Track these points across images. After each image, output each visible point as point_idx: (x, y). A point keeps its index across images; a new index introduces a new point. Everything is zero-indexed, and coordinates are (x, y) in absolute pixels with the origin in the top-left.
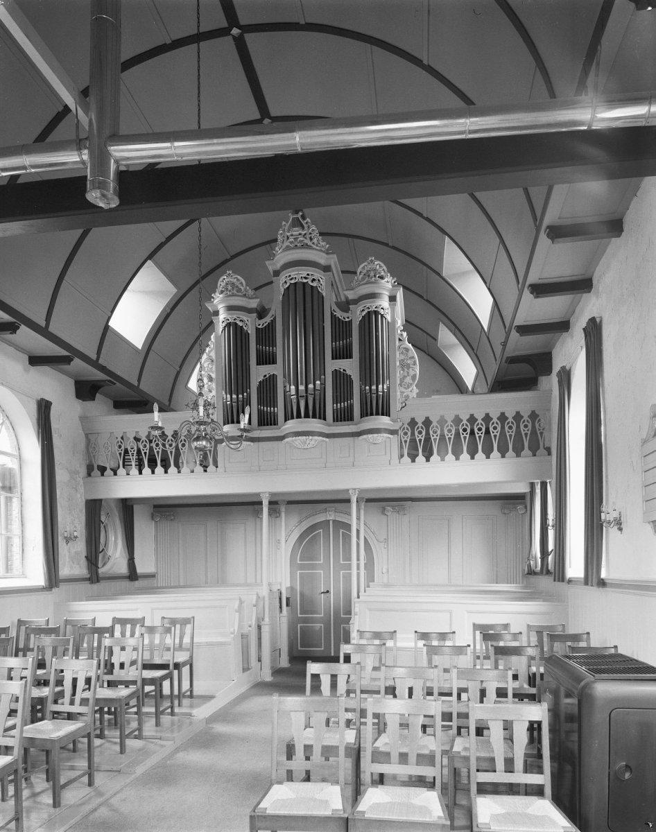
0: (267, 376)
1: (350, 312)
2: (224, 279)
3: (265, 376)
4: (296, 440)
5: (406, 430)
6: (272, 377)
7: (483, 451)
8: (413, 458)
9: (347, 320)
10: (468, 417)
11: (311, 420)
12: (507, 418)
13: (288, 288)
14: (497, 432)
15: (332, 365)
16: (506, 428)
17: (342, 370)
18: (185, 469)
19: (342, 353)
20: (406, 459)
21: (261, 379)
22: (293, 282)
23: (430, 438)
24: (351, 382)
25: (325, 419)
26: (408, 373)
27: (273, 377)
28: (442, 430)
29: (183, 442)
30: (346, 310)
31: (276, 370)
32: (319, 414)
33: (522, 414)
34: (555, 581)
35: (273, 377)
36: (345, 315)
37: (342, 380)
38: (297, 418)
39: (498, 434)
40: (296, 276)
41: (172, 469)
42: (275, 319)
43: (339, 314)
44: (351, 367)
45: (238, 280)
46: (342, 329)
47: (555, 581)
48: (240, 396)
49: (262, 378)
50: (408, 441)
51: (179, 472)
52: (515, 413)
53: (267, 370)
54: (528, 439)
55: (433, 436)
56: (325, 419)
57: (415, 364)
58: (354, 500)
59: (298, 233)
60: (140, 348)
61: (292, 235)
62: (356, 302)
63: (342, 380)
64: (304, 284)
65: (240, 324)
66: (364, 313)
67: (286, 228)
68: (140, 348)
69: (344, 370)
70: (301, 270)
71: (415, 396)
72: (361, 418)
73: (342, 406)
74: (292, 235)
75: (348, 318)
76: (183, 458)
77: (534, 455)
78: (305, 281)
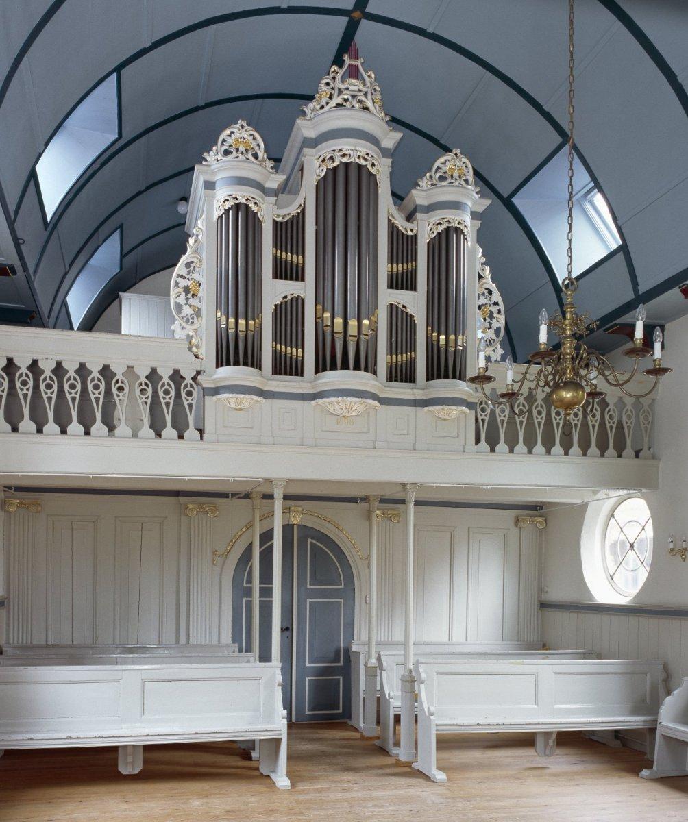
0: (289, 298)
1: (415, 222)
2: (233, 132)
3: (286, 297)
4: (338, 402)
5: (143, 387)
6: (294, 300)
7: (524, 443)
8: (493, 443)
9: (410, 233)
10: (148, 372)
11: (362, 373)
12: (183, 378)
13: (335, 169)
14: (486, 416)
15: (387, 296)
16: (18, 384)
17: (401, 306)
18: (122, 429)
19: (403, 282)
20: (484, 445)
21: (279, 300)
22: (345, 160)
23: (65, 398)
24: (413, 327)
25: (375, 373)
26: (490, 324)
27: (298, 302)
28: (620, 416)
29: (629, 413)
30: (409, 218)
31: (305, 289)
32: (253, 361)
33: (182, 373)
34: (240, 651)
35: (298, 302)
36: (409, 226)
37: (400, 320)
38: (234, 365)
39: (78, 396)
40: (351, 153)
41: (99, 427)
42: (303, 211)
43: (400, 222)
44: (415, 302)
45: (254, 139)
46: (402, 245)
47: (240, 651)
48: (251, 322)
49: (281, 300)
50: (579, 425)
51: (87, 433)
52: (150, 370)
53: (289, 288)
54: (192, 415)
55: (537, 418)
56: (375, 373)
57: (499, 311)
58: (278, 494)
59: (356, 88)
60: (640, 293)
61: (348, 89)
62: (430, 209)
63: (400, 320)
64: (359, 166)
65: (255, 208)
66: (441, 228)
67: (339, 77)
68: (640, 293)
69: (404, 306)
70: (360, 145)
71: (499, 359)
72: (217, 367)
73: (399, 360)
74: (348, 89)
75: (412, 230)
76: (120, 413)
77: (620, 456)
78: (363, 163)
